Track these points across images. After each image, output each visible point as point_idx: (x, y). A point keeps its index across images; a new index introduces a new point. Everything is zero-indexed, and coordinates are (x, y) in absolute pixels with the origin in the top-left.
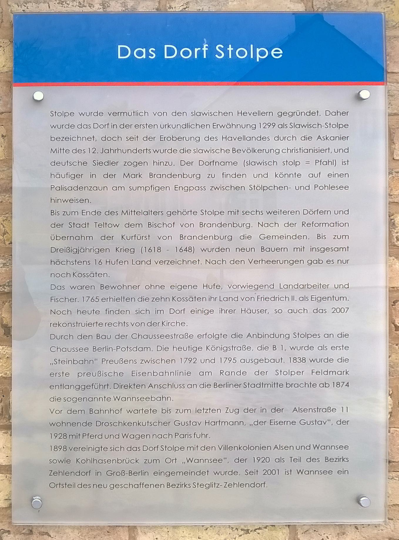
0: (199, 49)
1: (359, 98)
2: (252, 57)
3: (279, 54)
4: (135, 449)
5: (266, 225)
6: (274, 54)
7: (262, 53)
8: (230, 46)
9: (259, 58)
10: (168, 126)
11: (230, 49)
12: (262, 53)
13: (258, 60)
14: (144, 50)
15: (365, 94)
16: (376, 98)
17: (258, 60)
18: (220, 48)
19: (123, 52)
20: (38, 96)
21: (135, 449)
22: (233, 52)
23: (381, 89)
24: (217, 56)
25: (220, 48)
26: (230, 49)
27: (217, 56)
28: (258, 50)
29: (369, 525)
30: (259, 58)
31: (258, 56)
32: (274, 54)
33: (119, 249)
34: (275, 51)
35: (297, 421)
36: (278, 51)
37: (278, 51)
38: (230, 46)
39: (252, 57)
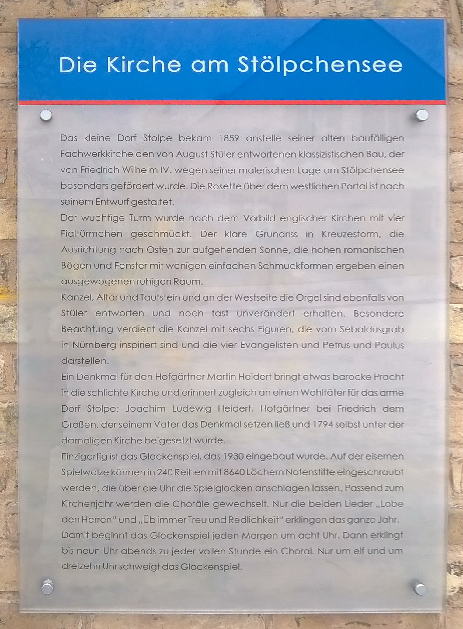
0: (133, 61)
1: (415, 119)
2: (279, 70)
3: (382, 68)
4: (130, 457)
5: (229, 267)
6: (171, 67)
7: (290, 66)
8: (255, 58)
9: (287, 72)
10: (102, 154)
11: (255, 61)
12: (290, 66)
13: (285, 75)
14: (203, 63)
15: (422, 114)
16: (438, 120)
17: (285, 75)
18: (243, 60)
19: (69, 65)
20: (46, 115)
21: (130, 457)
22: (258, 65)
23: (441, 109)
24: (240, 69)
25: (243, 60)
26: (255, 61)
27: (240, 69)
28: (285, 63)
29: (249, 615)
30: (287, 72)
31: (285, 70)
32: (171, 67)
33: (326, 234)
34: (336, 64)
35: (171, 503)
36: (340, 64)
37: (340, 64)
38: (255, 58)
39: (279, 70)
